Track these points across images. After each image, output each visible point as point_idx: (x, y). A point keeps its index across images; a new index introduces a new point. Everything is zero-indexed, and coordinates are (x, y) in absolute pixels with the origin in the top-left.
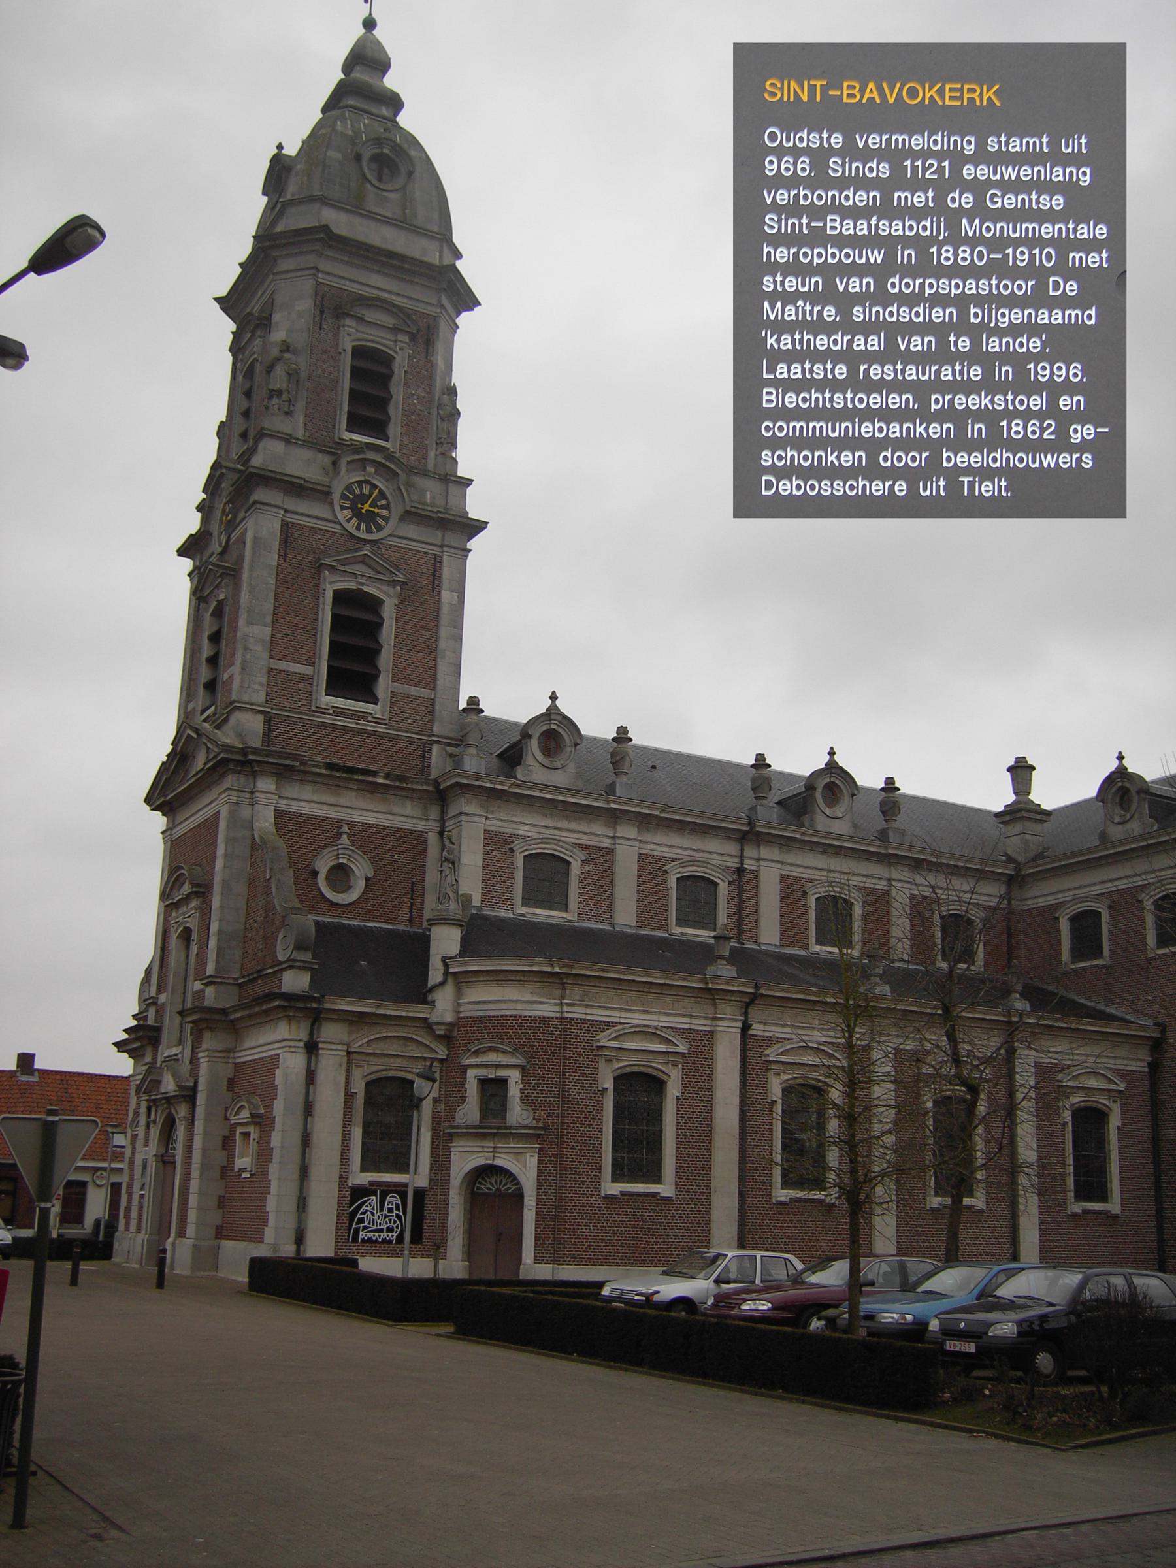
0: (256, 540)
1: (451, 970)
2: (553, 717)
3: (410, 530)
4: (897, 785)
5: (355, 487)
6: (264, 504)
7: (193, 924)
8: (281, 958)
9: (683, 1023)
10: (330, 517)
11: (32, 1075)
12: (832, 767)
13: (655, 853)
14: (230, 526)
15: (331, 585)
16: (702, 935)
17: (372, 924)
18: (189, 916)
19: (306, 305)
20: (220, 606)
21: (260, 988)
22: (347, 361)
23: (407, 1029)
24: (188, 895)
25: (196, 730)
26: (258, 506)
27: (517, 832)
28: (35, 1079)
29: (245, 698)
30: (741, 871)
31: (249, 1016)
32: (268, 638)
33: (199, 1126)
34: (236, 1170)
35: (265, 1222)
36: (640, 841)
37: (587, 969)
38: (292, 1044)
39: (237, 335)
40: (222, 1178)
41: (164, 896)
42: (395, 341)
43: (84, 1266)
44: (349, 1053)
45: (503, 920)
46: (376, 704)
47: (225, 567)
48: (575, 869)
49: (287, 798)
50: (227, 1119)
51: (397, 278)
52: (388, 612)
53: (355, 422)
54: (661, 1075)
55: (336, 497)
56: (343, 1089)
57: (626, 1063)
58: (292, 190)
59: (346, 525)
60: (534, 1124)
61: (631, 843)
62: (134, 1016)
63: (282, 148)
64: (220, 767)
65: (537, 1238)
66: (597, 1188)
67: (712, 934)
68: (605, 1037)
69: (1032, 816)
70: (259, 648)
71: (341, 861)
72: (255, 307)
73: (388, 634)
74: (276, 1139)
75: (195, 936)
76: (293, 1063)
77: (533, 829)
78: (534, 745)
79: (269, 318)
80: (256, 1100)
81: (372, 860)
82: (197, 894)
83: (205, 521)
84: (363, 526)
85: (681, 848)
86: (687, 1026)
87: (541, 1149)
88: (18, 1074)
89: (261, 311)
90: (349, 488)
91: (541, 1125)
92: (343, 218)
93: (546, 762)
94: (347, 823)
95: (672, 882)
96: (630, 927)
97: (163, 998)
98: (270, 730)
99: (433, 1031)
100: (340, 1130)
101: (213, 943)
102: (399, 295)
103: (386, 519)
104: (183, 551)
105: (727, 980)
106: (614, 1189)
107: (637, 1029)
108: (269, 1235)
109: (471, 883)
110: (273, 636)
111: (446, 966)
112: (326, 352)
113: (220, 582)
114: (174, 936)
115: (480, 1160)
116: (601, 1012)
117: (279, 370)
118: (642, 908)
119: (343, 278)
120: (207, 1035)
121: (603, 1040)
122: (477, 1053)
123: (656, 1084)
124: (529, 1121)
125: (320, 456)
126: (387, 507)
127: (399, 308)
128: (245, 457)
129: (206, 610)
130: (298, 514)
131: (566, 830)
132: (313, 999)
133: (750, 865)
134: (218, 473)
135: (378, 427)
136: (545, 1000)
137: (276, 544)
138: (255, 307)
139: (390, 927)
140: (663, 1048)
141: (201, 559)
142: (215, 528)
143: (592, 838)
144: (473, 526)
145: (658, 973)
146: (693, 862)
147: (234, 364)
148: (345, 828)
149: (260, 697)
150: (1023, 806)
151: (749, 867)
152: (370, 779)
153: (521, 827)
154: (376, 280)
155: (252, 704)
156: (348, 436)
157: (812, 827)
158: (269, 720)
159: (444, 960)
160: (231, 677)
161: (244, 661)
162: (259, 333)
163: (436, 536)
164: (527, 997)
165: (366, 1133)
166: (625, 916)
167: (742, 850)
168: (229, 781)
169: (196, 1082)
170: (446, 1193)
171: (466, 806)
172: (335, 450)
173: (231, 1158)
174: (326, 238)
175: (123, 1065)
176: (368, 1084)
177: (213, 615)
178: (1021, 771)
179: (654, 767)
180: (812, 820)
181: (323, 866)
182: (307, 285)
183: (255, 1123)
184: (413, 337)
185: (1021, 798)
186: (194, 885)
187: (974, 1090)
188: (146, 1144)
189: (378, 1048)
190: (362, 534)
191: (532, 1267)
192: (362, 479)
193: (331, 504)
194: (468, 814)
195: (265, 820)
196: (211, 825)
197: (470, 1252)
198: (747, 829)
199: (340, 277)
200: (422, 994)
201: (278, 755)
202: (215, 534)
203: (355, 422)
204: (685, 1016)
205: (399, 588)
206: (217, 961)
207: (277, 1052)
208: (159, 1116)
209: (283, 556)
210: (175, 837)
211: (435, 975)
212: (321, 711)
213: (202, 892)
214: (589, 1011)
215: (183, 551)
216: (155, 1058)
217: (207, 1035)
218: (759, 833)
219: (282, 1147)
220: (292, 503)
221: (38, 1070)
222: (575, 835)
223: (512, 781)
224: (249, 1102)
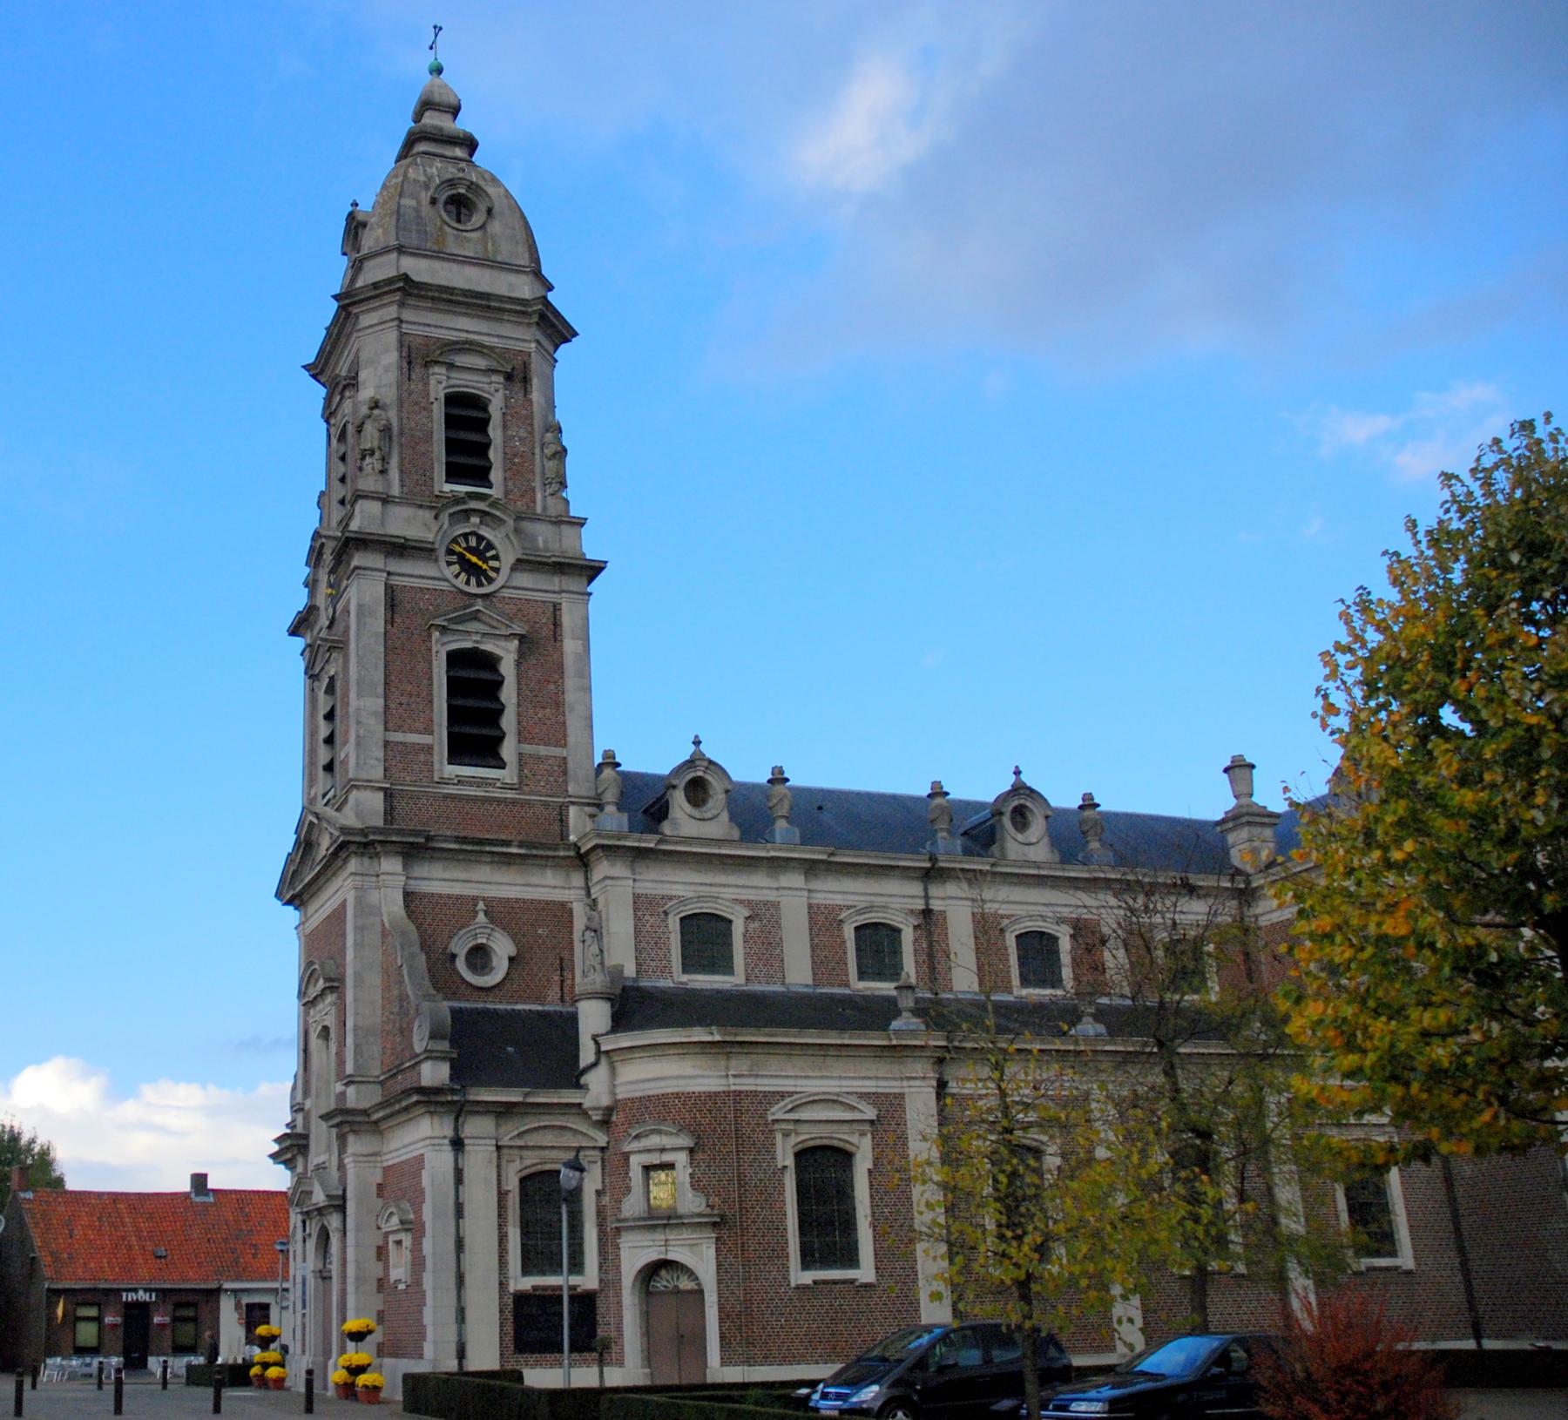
0: (360, 606)
1: (603, 1048)
2: (698, 763)
3: (524, 579)
4: (786, 775)
6: (365, 569)
7: (330, 1021)
8: (418, 1050)
9: (870, 1086)
11: (207, 1195)
12: (1020, 789)
13: (828, 902)
14: (334, 599)
16: (885, 988)
17: (519, 1007)
18: (325, 1012)
19: (392, 358)
20: (332, 679)
21: (403, 1082)
22: (439, 411)
23: (561, 1118)
24: (324, 990)
25: (317, 815)
27: (668, 893)
28: (211, 1199)
29: (363, 776)
30: (927, 913)
31: (392, 1115)
32: (381, 710)
33: (350, 1235)
34: (392, 1281)
35: (422, 1335)
36: (810, 891)
37: (754, 1035)
38: (436, 1141)
39: (328, 400)
40: (379, 1291)
41: (302, 993)
43: (228, 1393)
44: (498, 1148)
45: (663, 991)
46: (504, 768)
47: (333, 641)
48: (738, 929)
49: (416, 878)
50: (379, 1228)
51: (484, 318)
52: (507, 668)
53: (454, 473)
54: (848, 1147)
56: (495, 1187)
57: (807, 1136)
58: (369, 241)
59: (454, 581)
60: (708, 1211)
61: (799, 893)
62: (287, 1125)
63: (357, 205)
64: (341, 850)
65: (722, 1338)
66: (786, 1277)
67: (893, 985)
68: (781, 1109)
69: (1258, 819)
70: (372, 721)
71: (480, 941)
72: (343, 369)
73: (508, 694)
74: (427, 1246)
75: (333, 1035)
76: (440, 1162)
77: (687, 887)
78: (1007, 821)
79: (356, 377)
80: (406, 1205)
81: (513, 937)
82: (332, 989)
83: (312, 595)
84: (473, 580)
85: (856, 894)
86: (873, 1090)
87: (718, 1239)
88: (193, 1196)
89: (349, 371)
91: (716, 1212)
92: (423, 264)
93: (696, 813)
94: (484, 899)
95: (849, 933)
96: (807, 986)
97: (308, 1104)
98: (392, 808)
99: (589, 1117)
100: (496, 1232)
101: (350, 1040)
102: (489, 335)
103: (497, 570)
104: (294, 631)
105: (913, 1033)
106: (808, 1277)
107: (816, 1098)
108: (428, 1349)
109: (623, 956)
110: (386, 707)
111: (597, 1044)
112: (417, 403)
114: (313, 1036)
115: (653, 1255)
116: (772, 1081)
117: (370, 429)
118: (816, 964)
119: (429, 325)
120: (351, 1138)
121: (777, 1112)
122: (637, 1137)
123: (843, 1157)
124: (702, 1208)
125: (420, 512)
127: (491, 348)
128: (345, 522)
129: (320, 688)
130: (403, 575)
131: (724, 886)
132: (453, 1091)
133: (936, 905)
134: (318, 545)
135: (480, 475)
136: (706, 1073)
137: (381, 611)
138: (343, 369)
139: (540, 1008)
140: (848, 1116)
142: (321, 601)
143: (754, 891)
144: (592, 568)
145: (834, 1033)
146: (870, 908)
147: (328, 430)
148: (481, 905)
149: (378, 773)
150: (1244, 810)
151: (935, 908)
152: (504, 850)
153: (674, 887)
154: (464, 323)
155: (370, 781)
156: (448, 487)
157: (1004, 857)
158: (389, 795)
159: (595, 1038)
160: (347, 756)
161: (358, 736)
162: (347, 394)
163: (556, 582)
164: (689, 1071)
165: (525, 1233)
166: (798, 974)
167: (926, 890)
168: (353, 864)
169: (345, 1190)
170: (618, 1295)
171: (603, 868)
172: (437, 504)
173: (386, 1269)
174: (407, 289)
175: (278, 1179)
176: (523, 1181)
177: (326, 692)
178: (1239, 769)
179: (820, 808)
180: (1003, 848)
181: (460, 947)
182: (392, 336)
183: (407, 1230)
184: (509, 377)
185: (1244, 800)
186: (327, 980)
187: (1205, 1135)
188: (304, 1261)
189: (532, 1140)
190: (473, 589)
191: (719, 1371)
194: (613, 878)
195: (393, 905)
196: (339, 915)
197: (649, 1357)
198: (928, 865)
199: (425, 325)
200: (572, 1076)
201: (401, 832)
202: (322, 608)
203: (454, 473)
204: (870, 1078)
206: (356, 1060)
207: (422, 1151)
208: (313, 1228)
209: (390, 621)
210: (308, 931)
211: (586, 1055)
212: (444, 782)
213: (335, 985)
214: (759, 1081)
215: (294, 631)
216: (306, 1168)
217: (351, 1138)
218: (942, 869)
219: (434, 1254)
220: (396, 565)
221: (213, 1190)
222: (736, 890)
223: (658, 837)
224: (397, 1206)
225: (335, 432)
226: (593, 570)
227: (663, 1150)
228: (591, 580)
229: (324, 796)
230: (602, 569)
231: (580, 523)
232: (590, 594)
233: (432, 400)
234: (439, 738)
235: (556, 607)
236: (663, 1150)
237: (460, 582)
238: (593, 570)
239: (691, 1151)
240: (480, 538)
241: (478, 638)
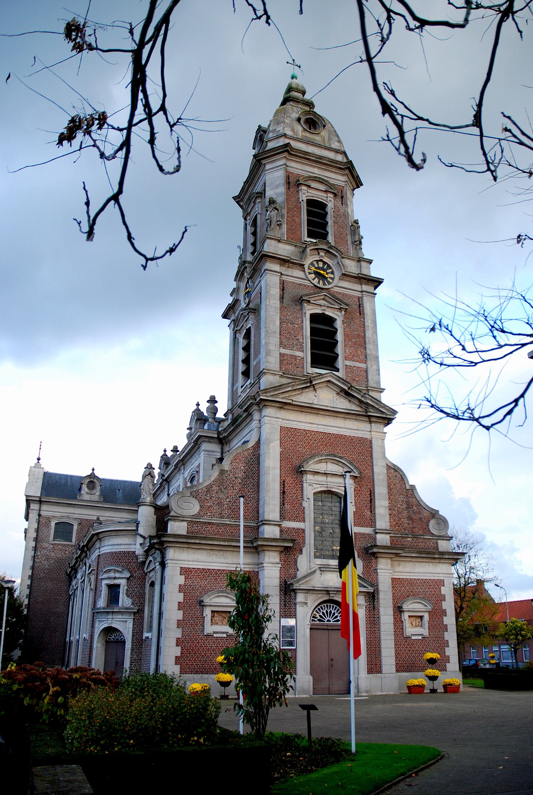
5: (315, 263)
10: (304, 277)
15: (309, 310)
20: (249, 331)
26: (266, 271)
42: (327, 197)
52: (339, 324)
55: (306, 267)
73: (340, 336)
84: (321, 282)
90: (312, 264)
103: (333, 279)
113: (248, 318)
126: (332, 273)
135: (323, 236)
141: (235, 316)
156: (308, 240)
184: (335, 195)
190: (321, 285)
192: (319, 259)
193: (304, 271)
205: (343, 312)
215: (225, 316)
220: (284, 270)
225: (249, 222)
226: (377, 282)
227: (115, 578)
228: (376, 288)
229: (242, 387)
230: (382, 282)
231: (370, 262)
232: (376, 294)
233: (301, 201)
234: (307, 355)
235: (360, 299)
236: (115, 578)
237: (316, 282)
238: (377, 282)
239: (128, 579)
240: (324, 263)
241: (325, 308)
